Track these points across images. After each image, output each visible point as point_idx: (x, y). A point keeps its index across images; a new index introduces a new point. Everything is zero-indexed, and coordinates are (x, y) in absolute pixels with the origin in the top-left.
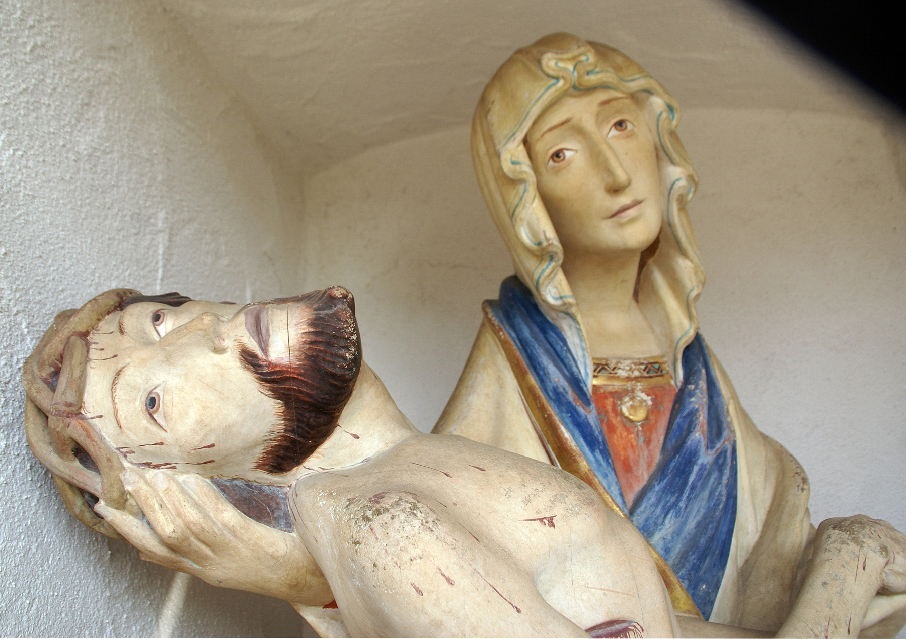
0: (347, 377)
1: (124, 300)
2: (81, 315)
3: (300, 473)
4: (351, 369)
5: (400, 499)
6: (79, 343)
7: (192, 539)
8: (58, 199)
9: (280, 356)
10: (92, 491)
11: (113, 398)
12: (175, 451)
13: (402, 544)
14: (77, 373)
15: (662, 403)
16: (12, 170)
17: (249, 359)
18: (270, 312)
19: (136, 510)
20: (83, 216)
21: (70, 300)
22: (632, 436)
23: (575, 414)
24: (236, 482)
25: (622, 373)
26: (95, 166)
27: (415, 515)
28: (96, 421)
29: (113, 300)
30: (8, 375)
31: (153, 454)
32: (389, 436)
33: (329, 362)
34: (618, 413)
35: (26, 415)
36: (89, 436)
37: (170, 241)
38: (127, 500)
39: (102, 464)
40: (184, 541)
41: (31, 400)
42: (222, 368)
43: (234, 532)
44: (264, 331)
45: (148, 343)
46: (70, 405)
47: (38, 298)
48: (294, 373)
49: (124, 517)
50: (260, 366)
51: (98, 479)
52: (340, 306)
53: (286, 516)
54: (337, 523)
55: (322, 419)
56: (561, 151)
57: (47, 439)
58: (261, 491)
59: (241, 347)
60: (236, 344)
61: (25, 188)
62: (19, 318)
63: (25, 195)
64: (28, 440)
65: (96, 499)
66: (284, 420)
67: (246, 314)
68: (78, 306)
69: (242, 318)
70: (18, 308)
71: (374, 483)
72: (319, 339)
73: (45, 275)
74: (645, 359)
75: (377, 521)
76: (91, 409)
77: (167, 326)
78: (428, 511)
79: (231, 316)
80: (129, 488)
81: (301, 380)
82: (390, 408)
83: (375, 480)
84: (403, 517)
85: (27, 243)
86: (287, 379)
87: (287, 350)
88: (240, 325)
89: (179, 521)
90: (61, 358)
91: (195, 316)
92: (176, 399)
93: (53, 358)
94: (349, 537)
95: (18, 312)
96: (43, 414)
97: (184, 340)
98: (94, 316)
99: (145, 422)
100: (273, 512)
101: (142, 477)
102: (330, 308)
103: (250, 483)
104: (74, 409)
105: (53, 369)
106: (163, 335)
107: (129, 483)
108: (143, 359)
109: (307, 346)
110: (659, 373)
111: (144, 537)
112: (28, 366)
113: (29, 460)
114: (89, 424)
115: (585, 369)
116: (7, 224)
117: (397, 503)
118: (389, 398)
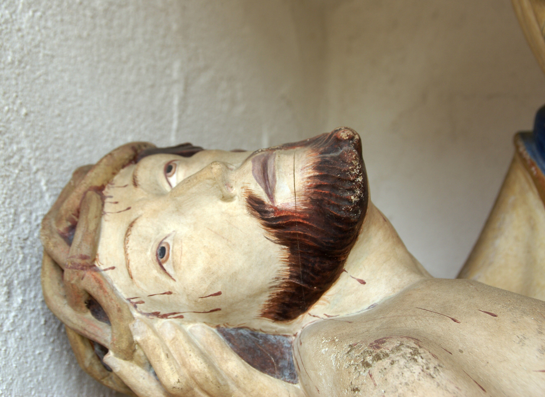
0: (353, 220)
1: (138, 153)
2: (96, 171)
3: (305, 320)
4: (356, 212)
5: (401, 344)
6: (95, 197)
7: (196, 390)
8: (75, 57)
9: (286, 202)
10: (102, 342)
11: (125, 249)
12: (183, 300)
13: (400, 391)
14: (92, 226)
16: (32, 31)
17: (256, 206)
18: (277, 158)
19: (143, 360)
20: (100, 71)
21: (87, 156)
24: (241, 331)
26: (111, 20)
27: (416, 360)
28: (109, 273)
29: (128, 154)
30: (27, 232)
31: (161, 303)
32: (396, 281)
33: (334, 205)
35: (43, 269)
36: (101, 287)
37: (186, 90)
38: (135, 351)
39: (113, 315)
40: (188, 391)
41: (48, 254)
42: (230, 216)
43: (237, 382)
44: (270, 177)
45: (160, 194)
46: (84, 258)
47: (57, 155)
48: (299, 217)
49: (132, 368)
50: (266, 212)
51: (108, 330)
52: (345, 148)
53: (291, 366)
54: (337, 370)
55: (327, 264)
57: (62, 292)
58: (266, 340)
59: (247, 195)
60: (243, 191)
61: (44, 48)
62: (39, 176)
63: (45, 55)
64: (44, 294)
65: (105, 351)
66: (289, 265)
67: (254, 161)
68: (95, 161)
69: (249, 165)
70: (39, 166)
71: (377, 329)
72: (325, 182)
73: (64, 133)
75: (377, 366)
76: (104, 261)
77: (177, 178)
78: (430, 356)
79: (240, 164)
80: (137, 338)
81: (306, 225)
82: (399, 252)
83: (378, 326)
84: (402, 362)
85: (47, 103)
86: (293, 224)
87: (293, 195)
88: (248, 172)
89: (184, 371)
90: (78, 213)
91: (205, 165)
92: (185, 249)
93: (70, 213)
94: (348, 383)
95: (38, 170)
96: (59, 267)
97: (194, 190)
98: (110, 170)
99: (155, 272)
100: (277, 362)
101: (151, 326)
102: (336, 150)
103: (256, 332)
104: (88, 261)
105: (69, 224)
106: (174, 185)
107: (138, 333)
108: (155, 211)
109: (313, 190)
111: (150, 389)
112: (47, 222)
113: (43, 315)
114: (102, 276)
116: (28, 85)
117: (398, 349)
118: (399, 241)
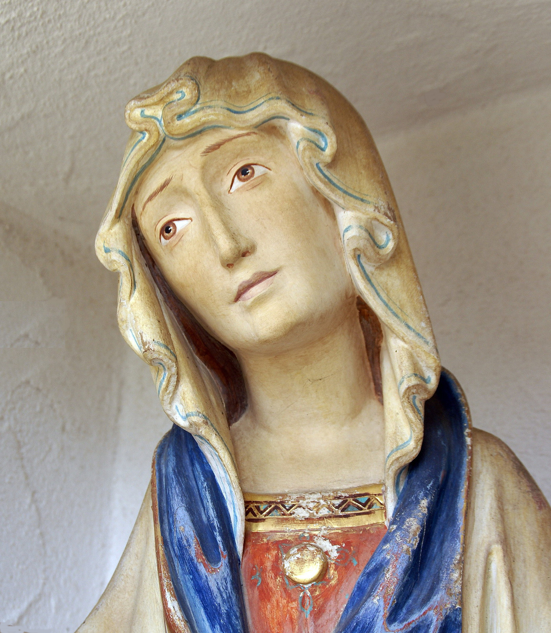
15: (357, 554)
22: (294, 605)
23: (196, 575)
25: (301, 513)
34: (278, 570)
56: (171, 222)
74: (345, 491)
110: (366, 510)
115: (234, 511)
